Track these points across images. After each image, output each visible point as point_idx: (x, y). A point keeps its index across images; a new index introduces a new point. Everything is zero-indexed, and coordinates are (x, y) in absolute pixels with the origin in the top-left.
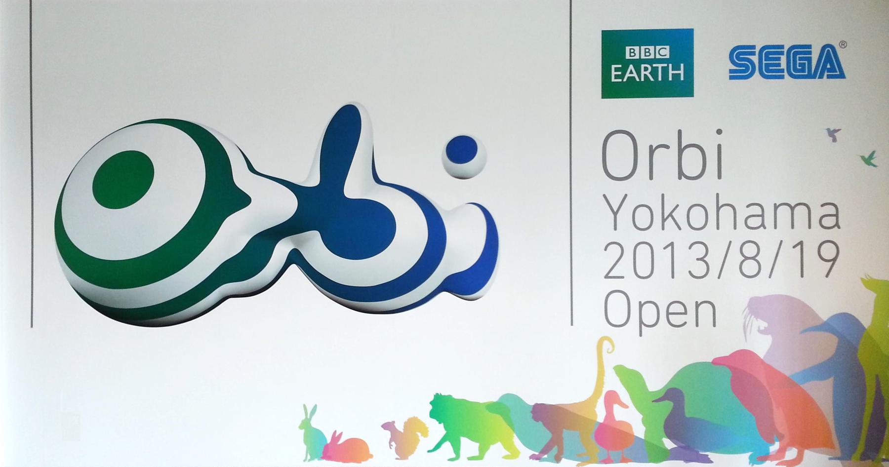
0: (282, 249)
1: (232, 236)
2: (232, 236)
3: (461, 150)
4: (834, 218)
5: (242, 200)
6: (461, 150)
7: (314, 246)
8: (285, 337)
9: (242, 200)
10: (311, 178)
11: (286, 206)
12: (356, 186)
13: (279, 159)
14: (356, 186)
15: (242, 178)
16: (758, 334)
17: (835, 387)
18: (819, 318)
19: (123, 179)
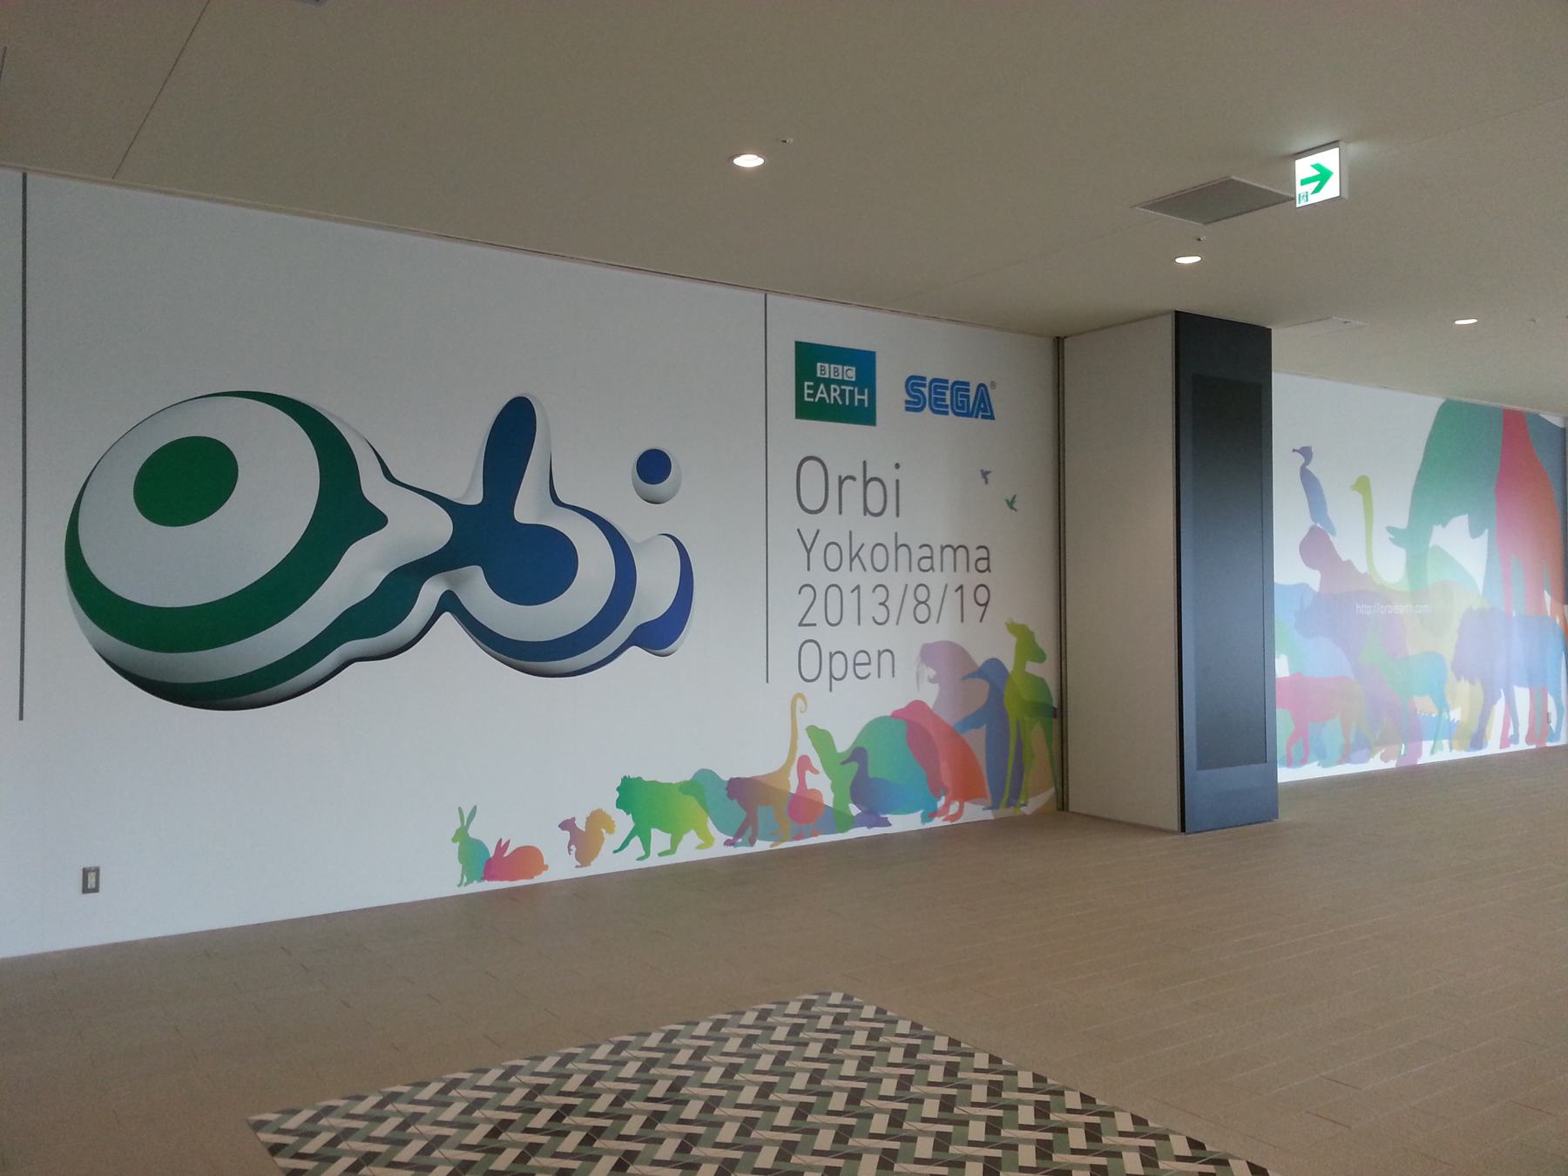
0: (431, 591)
1: (359, 572)
2: (359, 572)
5: (374, 520)
7: (476, 588)
9: (374, 520)
12: (528, 508)
13: (424, 475)
14: (528, 508)
15: (373, 488)
19: (187, 480)
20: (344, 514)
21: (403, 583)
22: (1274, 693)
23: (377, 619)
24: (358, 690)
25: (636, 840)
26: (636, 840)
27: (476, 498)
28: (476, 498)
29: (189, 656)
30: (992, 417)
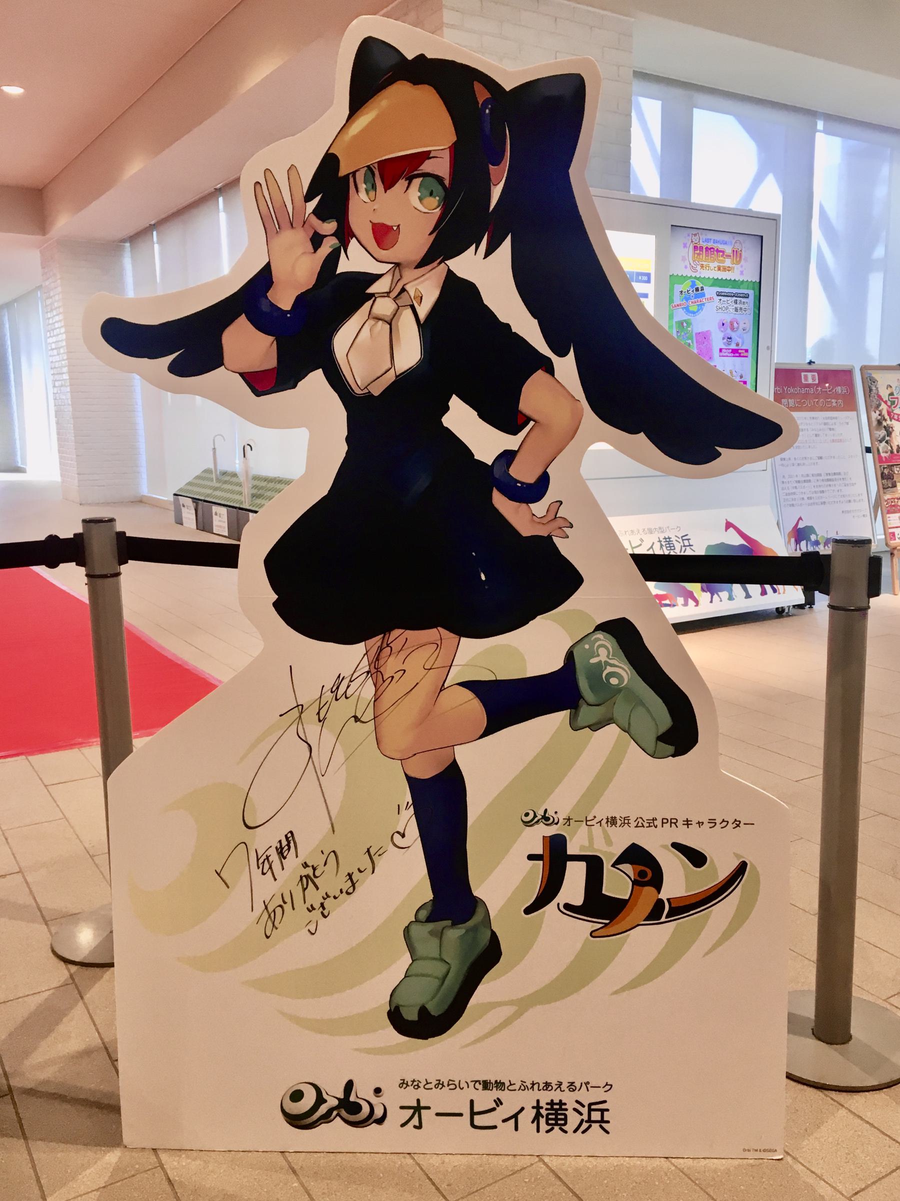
0: (335, 1113)
1: (536, 820)
2: (536, 820)
3: (378, 1091)
4: (476, 1110)
5: (326, 1101)
6: (378, 1091)
7: (343, 1113)
8: (335, 1134)
9: (326, 1101)
10: (341, 1095)
11: (335, 1102)
12: (352, 1098)
13: (540, 813)
14: (352, 1098)
15: (325, 1096)
16: (700, 602)
17: (777, 180)
18: (849, 155)
19: (527, 815)
20: (535, 816)
21: (330, 1111)
22: (174, 655)
23: (537, 822)
24: (536, 826)
25: (412, 1111)
26: (412, 1111)
27: (342, 1097)
28: (342, 1097)
29: (297, 1121)
30: (568, 537)
